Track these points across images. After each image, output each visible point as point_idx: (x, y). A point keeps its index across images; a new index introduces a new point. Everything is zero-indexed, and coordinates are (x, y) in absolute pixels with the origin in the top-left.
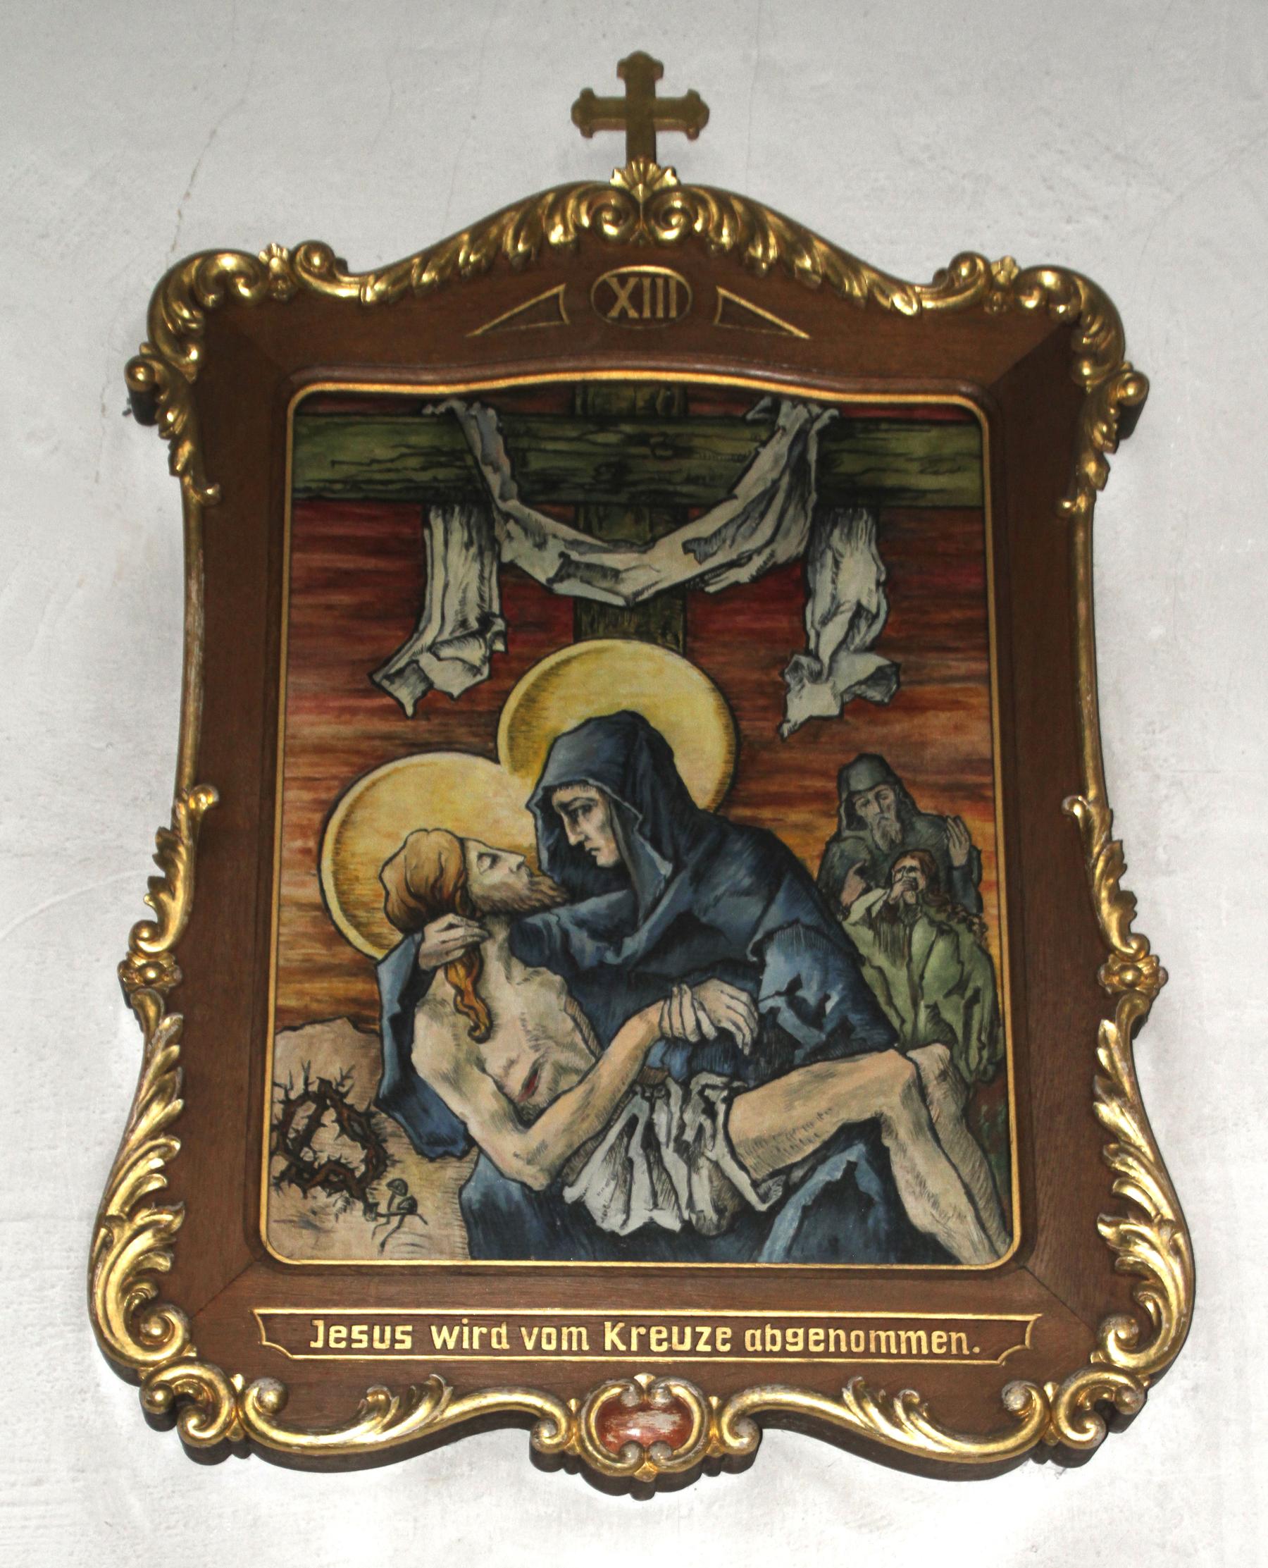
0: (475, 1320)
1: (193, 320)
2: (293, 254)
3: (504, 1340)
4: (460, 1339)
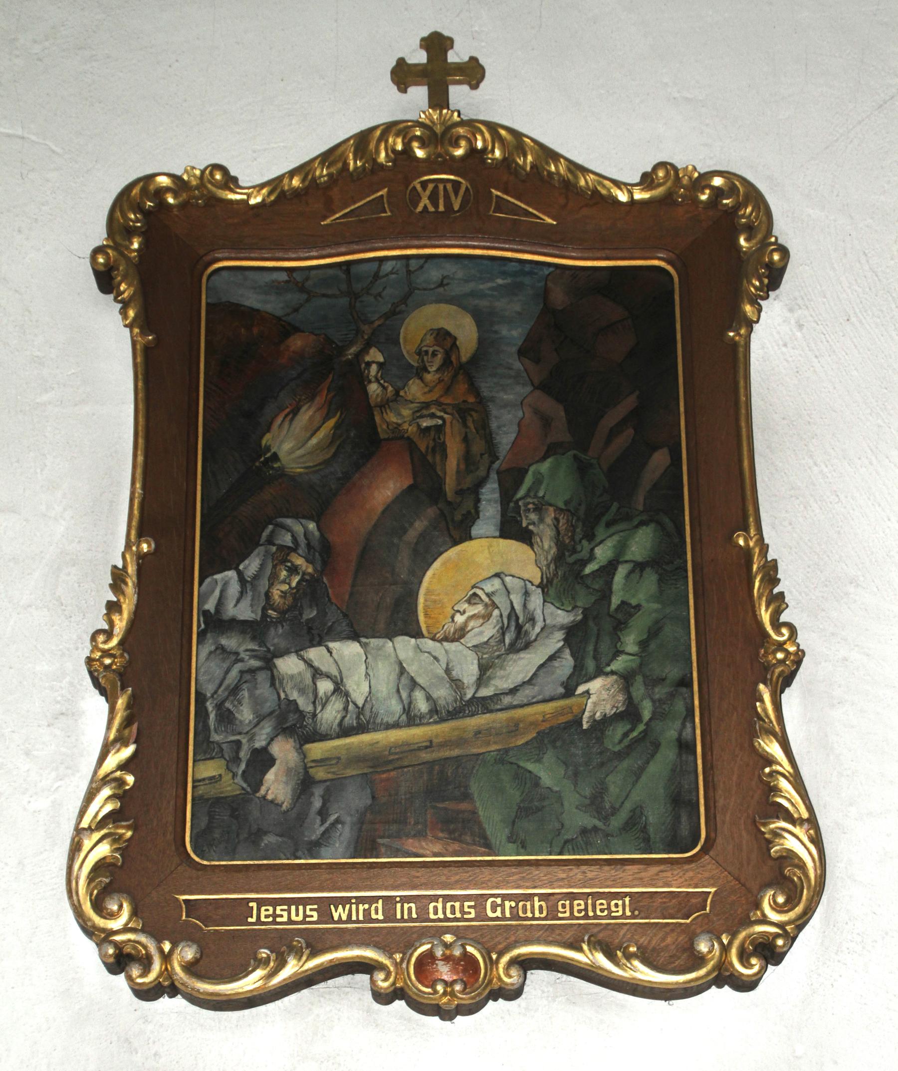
0: (361, 900)
1: (137, 220)
2: (203, 172)
3: (380, 911)
4: (350, 915)
